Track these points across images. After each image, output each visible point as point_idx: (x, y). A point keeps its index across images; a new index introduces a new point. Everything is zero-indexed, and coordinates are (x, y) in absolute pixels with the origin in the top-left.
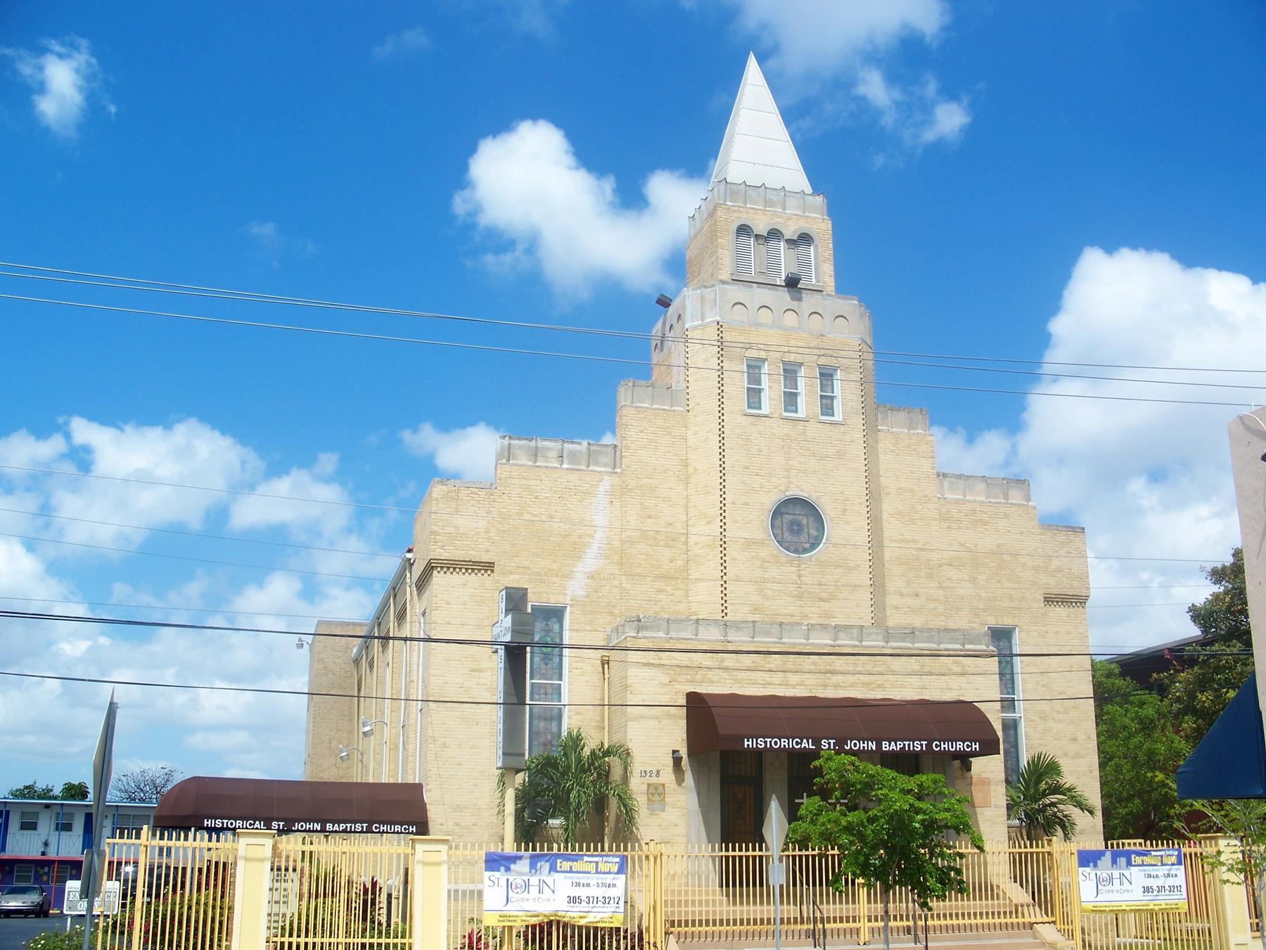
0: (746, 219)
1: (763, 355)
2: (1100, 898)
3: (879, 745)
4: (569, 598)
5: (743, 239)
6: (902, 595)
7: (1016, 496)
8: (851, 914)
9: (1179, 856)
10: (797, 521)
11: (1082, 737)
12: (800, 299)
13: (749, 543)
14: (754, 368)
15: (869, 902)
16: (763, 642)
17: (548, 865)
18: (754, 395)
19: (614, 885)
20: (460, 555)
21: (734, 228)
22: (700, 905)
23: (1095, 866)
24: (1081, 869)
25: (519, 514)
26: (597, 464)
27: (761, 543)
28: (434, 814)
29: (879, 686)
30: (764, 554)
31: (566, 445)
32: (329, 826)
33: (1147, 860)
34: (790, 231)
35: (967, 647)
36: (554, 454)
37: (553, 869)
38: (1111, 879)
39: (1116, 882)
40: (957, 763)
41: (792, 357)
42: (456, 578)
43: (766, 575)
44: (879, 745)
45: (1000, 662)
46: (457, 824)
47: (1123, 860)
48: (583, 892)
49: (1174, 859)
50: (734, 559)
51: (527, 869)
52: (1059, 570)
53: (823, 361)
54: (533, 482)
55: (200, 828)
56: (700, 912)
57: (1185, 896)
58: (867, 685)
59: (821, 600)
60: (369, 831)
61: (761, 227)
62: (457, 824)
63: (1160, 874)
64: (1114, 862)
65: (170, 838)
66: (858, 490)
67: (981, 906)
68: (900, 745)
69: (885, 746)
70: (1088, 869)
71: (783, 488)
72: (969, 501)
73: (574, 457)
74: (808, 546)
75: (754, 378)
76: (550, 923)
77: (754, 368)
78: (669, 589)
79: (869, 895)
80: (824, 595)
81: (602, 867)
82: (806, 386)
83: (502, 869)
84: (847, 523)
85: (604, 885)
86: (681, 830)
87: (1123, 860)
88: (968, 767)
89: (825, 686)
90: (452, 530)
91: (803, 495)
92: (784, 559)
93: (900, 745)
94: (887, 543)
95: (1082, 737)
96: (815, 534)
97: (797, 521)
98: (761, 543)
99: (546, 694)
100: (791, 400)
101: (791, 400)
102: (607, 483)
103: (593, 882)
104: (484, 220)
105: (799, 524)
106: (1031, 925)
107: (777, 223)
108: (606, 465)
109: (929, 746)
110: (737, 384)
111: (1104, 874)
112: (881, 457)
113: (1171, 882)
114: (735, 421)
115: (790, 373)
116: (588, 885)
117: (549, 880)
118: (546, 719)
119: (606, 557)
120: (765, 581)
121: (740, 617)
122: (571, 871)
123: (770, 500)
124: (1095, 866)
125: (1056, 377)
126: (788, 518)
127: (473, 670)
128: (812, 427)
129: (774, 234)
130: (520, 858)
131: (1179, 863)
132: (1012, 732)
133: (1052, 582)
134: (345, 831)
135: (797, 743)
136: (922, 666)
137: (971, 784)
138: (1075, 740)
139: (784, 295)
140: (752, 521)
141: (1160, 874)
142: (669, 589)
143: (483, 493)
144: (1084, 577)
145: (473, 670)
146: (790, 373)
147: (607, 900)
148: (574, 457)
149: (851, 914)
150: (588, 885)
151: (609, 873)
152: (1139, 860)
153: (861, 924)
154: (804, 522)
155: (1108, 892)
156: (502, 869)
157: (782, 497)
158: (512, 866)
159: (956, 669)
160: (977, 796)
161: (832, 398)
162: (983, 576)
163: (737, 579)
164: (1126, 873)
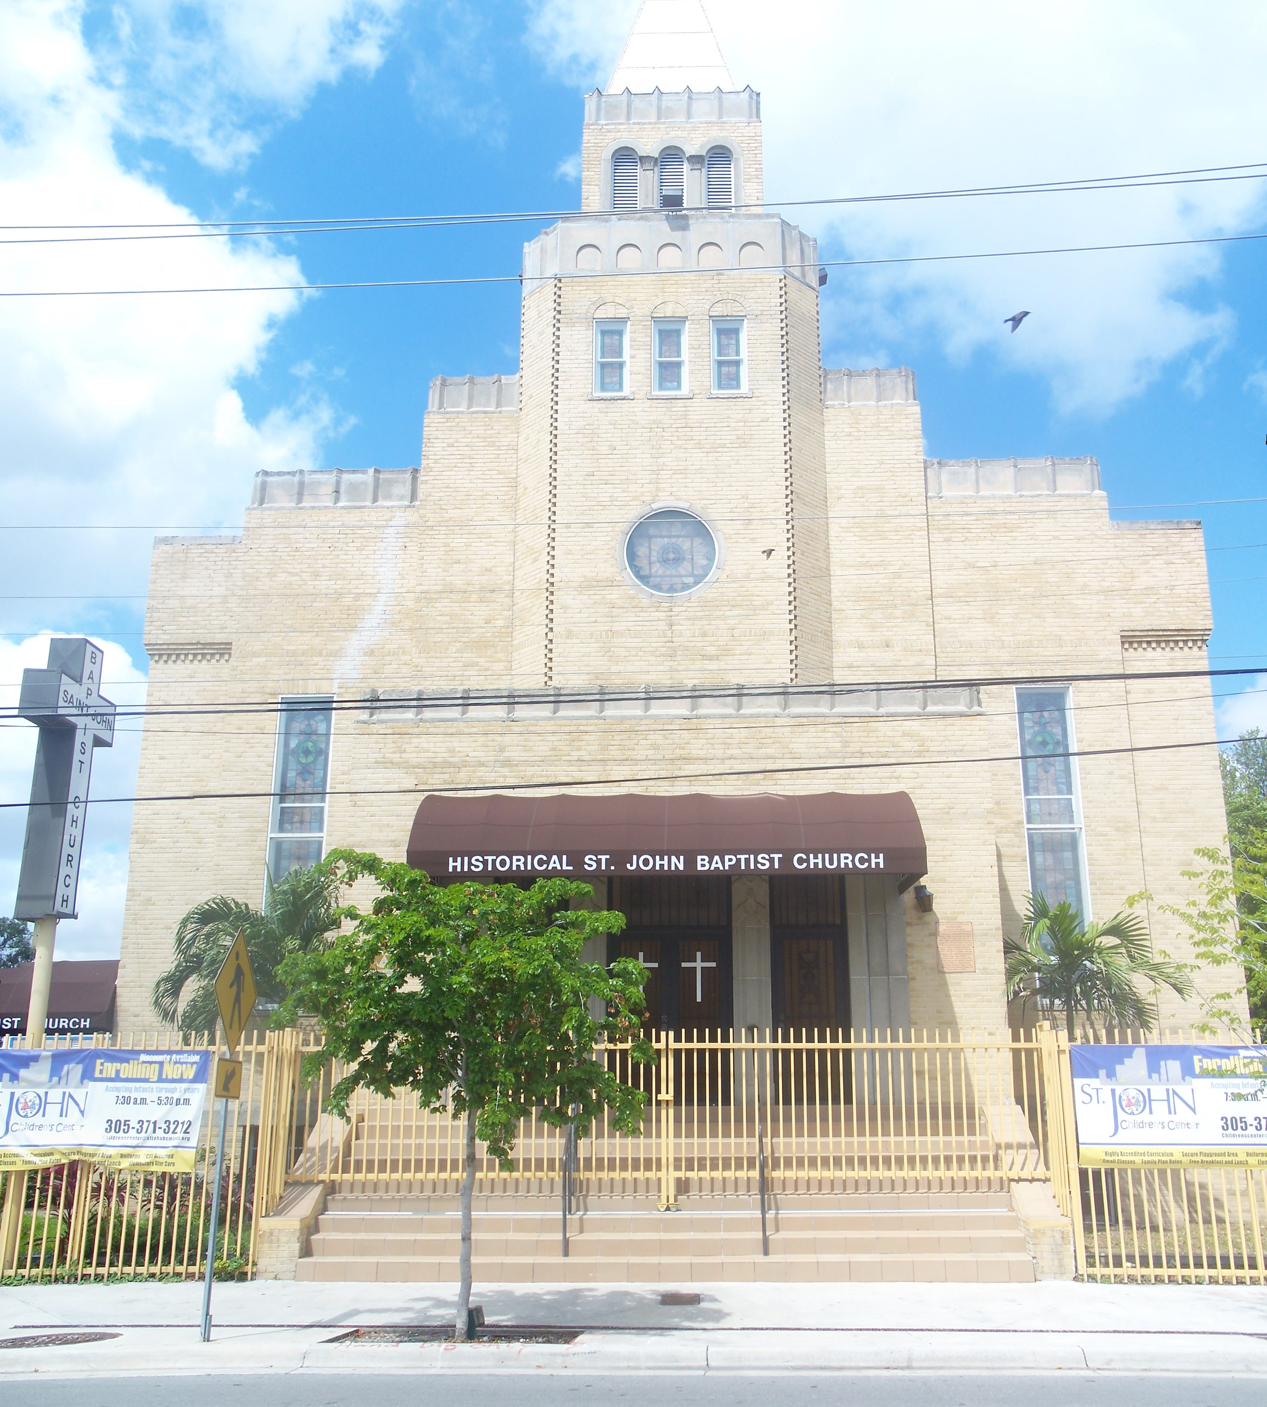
0: (625, 137)
1: (622, 313)
2: (1121, 1136)
3: (690, 862)
4: (336, 683)
5: (624, 169)
6: (861, 646)
8: (696, 1155)
12: (685, 228)
13: (589, 585)
14: (611, 332)
15: (677, 1134)
17: (80, 1068)
18: (610, 371)
19: (187, 1102)
20: (186, 636)
22: (396, 1135)
23: (1111, 1075)
24: (1078, 1082)
25: (272, 575)
26: (388, 497)
30: (614, 595)
31: (345, 476)
33: (126, 1070)
36: (330, 489)
37: (1188, 1071)
39: (1160, 1108)
41: (668, 311)
44: (690, 862)
45: (1067, 747)
48: (132, 1114)
50: (565, 608)
51: (45, 1077)
52: (1150, 590)
53: (718, 311)
56: (383, 1147)
66: (772, 492)
67: (960, 1145)
68: (730, 861)
69: (703, 864)
70: (1094, 1082)
71: (647, 498)
72: (983, 498)
73: (355, 490)
74: (691, 580)
76: (73, 1165)
77: (611, 332)
78: (481, 660)
79: (677, 1120)
80: (711, 650)
81: (170, 1071)
82: (696, 349)
83: (1102, 1073)
84: (753, 540)
87: (76, 1070)
91: (634, 513)
92: (645, 602)
93: (730, 861)
94: (835, 570)
96: (704, 562)
98: (611, 583)
99: (302, 822)
100: (669, 372)
101: (669, 372)
103: (151, 1096)
105: (676, 550)
106: (1004, 1185)
108: (402, 498)
109: (786, 861)
112: (830, 444)
115: (668, 333)
116: (144, 1101)
117: (79, 1094)
118: (299, 858)
122: (117, 1078)
124: (1111, 1075)
126: (658, 544)
131: (200, 1077)
132: (1068, 855)
135: (541, 862)
136: (846, 744)
137: (935, 934)
140: (595, 552)
142: (481, 660)
143: (222, 549)
146: (668, 333)
147: (170, 1126)
148: (355, 490)
149: (696, 1155)
150: (144, 1101)
151: (181, 1080)
152: (110, 1068)
153: (662, 1174)
154: (686, 545)
156: (1102, 1073)
157: (645, 510)
158: (23, 1073)
160: (948, 953)
161: (737, 363)
163: (569, 635)
164: (1183, 1090)
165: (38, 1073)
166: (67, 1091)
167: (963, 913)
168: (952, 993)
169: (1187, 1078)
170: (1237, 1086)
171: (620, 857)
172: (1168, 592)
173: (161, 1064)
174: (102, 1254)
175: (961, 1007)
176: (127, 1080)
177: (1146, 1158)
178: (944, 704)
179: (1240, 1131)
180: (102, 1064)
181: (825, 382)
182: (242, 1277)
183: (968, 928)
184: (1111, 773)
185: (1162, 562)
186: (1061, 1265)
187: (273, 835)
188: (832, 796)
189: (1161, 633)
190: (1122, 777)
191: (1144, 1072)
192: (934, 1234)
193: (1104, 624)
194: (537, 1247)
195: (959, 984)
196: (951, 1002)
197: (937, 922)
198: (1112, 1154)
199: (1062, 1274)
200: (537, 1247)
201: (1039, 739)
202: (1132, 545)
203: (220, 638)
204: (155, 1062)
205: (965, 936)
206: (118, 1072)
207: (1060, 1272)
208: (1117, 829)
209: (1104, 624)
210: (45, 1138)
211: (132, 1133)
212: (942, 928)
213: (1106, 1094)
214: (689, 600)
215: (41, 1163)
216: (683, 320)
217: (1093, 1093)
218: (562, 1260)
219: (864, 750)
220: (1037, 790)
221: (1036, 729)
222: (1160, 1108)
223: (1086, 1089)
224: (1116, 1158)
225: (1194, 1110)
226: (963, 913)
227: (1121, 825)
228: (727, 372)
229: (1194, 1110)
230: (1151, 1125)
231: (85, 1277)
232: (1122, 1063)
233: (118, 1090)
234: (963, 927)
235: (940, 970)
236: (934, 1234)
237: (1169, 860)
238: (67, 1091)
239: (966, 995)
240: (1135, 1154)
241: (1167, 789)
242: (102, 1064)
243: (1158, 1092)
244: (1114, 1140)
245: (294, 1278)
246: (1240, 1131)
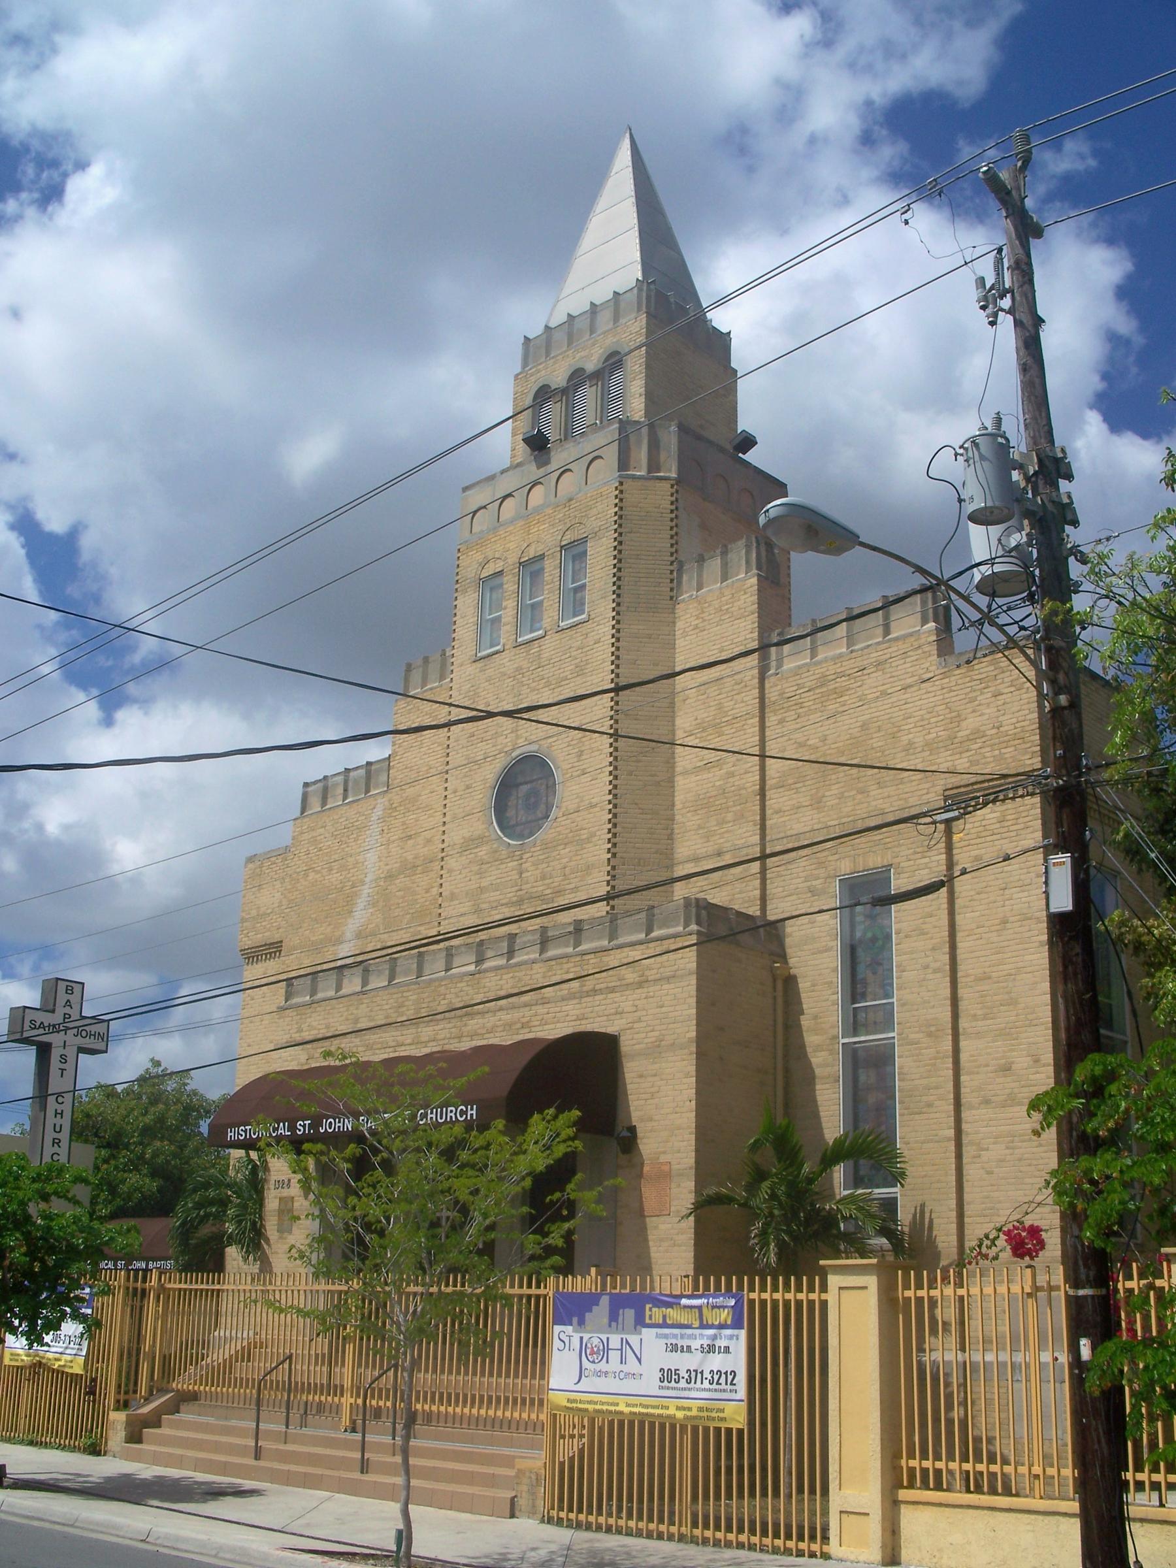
2: (584, 1385)
9: (737, 1310)
11: (1022, 1062)
23: (581, 1323)
27: (480, 840)
30: (483, 852)
33: (673, 1314)
38: (606, 1349)
39: (614, 1356)
43: (485, 883)
47: (629, 1314)
48: (683, 1363)
49: (725, 1316)
52: (977, 734)
57: (742, 1393)
58: (509, 1026)
63: (696, 1344)
64: (613, 1317)
65: (799, 1289)
70: (569, 1329)
83: (575, 1320)
87: (629, 1314)
89: (460, 1038)
95: (1022, 1062)
111: (594, 1339)
113: (716, 1362)
119: (374, 905)
120: (482, 890)
122: (664, 1325)
124: (581, 1323)
131: (737, 1325)
133: (962, 764)
137: (640, 1175)
138: (1007, 1069)
141: (696, 1344)
152: (656, 1314)
155: (599, 1374)
156: (575, 1320)
160: (649, 1193)
162: (835, 790)
164: (634, 1339)
165: (602, 1309)
166: (624, 1336)
167: (664, 1153)
168: (650, 1237)
169: (638, 1327)
170: (675, 1336)
172: (994, 731)
173: (700, 1308)
174: (590, 1506)
175: (657, 1252)
176: (673, 1326)
177: (598, 1407)
178: (668, 927)
179: (673, 1384)
180: (650, 1310)
181: (680, 577)
183: (666, 1168)
184: (927, 967)
185: (989, 695)
186: (534, 1506)
187: (846, 1040)
188: (264, 1079)
189: (986, 784)
190: (935, 971)
191: (606, 1320)
192: (490, 1470)
193: (927, 786)
194: (232, 1450)
195: (656, 1228)
196: (648, 1247)
197: (642, 1164)
198: (575, 1401)
199: (534, 1513)
200: (232, 1450)
201: (869, 935)
202: (960, 682)
204: (694, 1307)
205: (665, 1175)
206: (664, 1317)
207: (532, 1513)
208: (930, 1035)
209: (927, 786)
211: (683, 1384)
212: (646, 1169)
214: (534, 846)
216: (542, 557)
217: (567, 1340)
218: (253, 1462)
219: (598, 987)
220: (864, 997)
221: (867, 923)
223: (562, 1336)
224: (574, 1405)
225: (639, 1360)
226: (664, 1153)
227: (933, 1029)
228: (575, 599)
229: (639, 1360)
230: (606, 1373)
232: (591, 1311)
233: (666, 1336)
234: (663, 1167)
235: (641, 1214)
236: (490, 1470)
237: (987, 1065)
238: (624, 1336)
239: (661, 1240)
240: (590, 1402)
241: (990, 978)
242: (650, 1310)
244: (578, 1387)
246: (673, 1384)
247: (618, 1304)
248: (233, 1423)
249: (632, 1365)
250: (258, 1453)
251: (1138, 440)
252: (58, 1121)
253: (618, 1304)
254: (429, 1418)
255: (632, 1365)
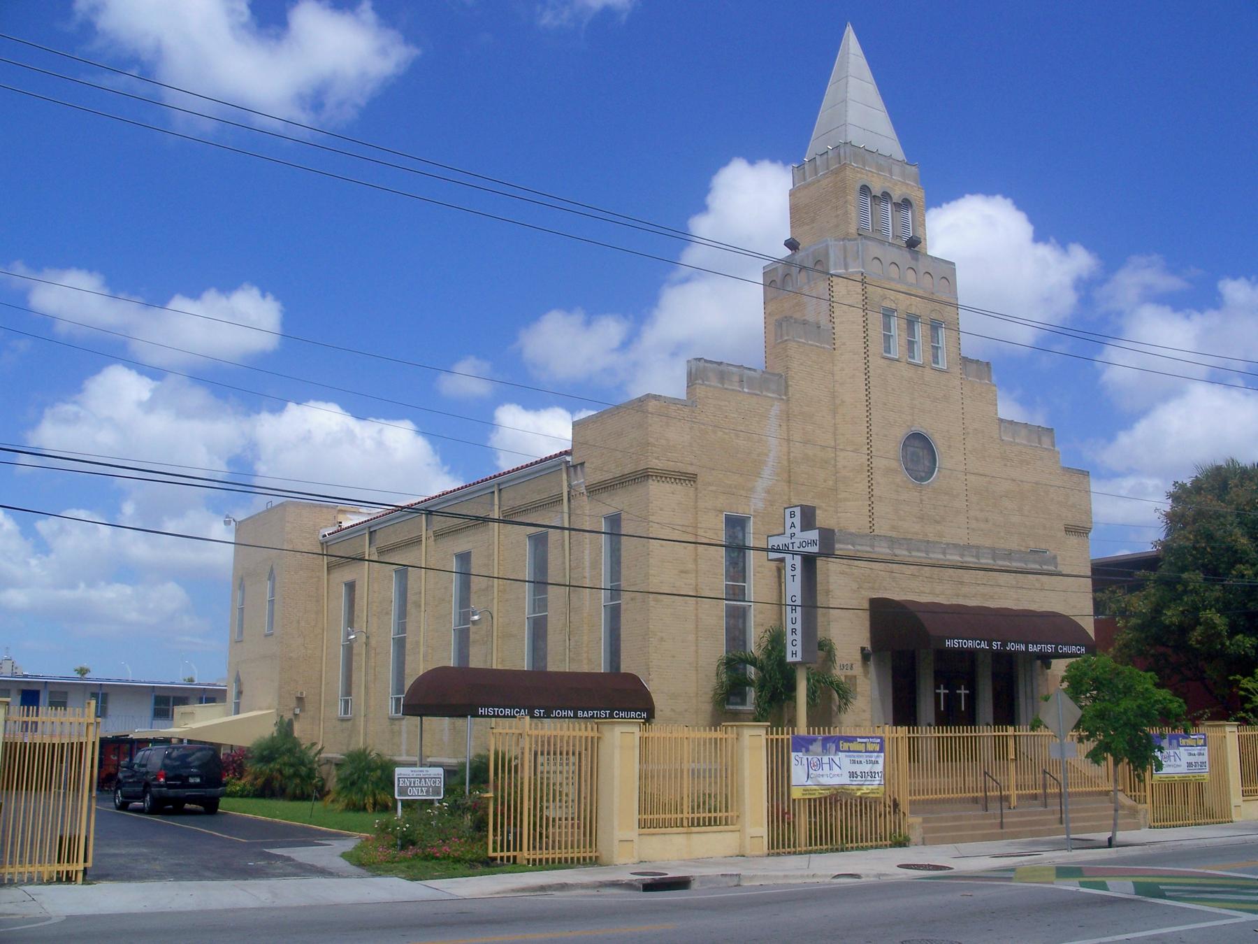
3: (1027, 648)
6: (977, 520)
7: (1046, 442)
10: (920, 452)
12: (917, 260)
16: (919, 555)
20: (671, 466)
21: (858, 187)
28: (659, 701)
29: (992, 597)
32: (580, 713)
33: (853, 746)
34: (897, 195)
35: (1045, 567)
36: (736, 378)
39: (826, 767)
40: (1039, 662)
42: (667, 487)
46: (673, 710)
48: (857, 768)
51: (820, 749)
54: (723, 403)
55: (475, 715)
59: (936, 521)
60: (611, 716)
61: (877, 189)
62: (673, 710)
63: (863, 760)
64: (824, 747)
69: (1011, 647)
70: (800, 754)
75: (887, 327)
80: (938, 518)
85: (871, 762)
86: (867, 715)
88: (1048, 666)
90: (663, 442)
91: (923, 431)
97: (920, 452)
102: (776, 409)
104: (105, 22)
107: (887, 186)
110: (876, 332)
114: (876, 362)
117: (836, 759)
121: (882, 533)
123: (900, 433)
125: (702, 272)
127: (682, 572)
128: (928, 371)
129: (886, 196)
130: (815, 740)
131: (881, 750)
134: (592, 717)
139: (906, 254)
144: (1088, 512)
145: (682, 572)
147: (873, 775)
152: (846, 746)
156: (1090, 745)
159: (1038, 585)
164: (836, 759)
165: (816, 747)
171: (1004, 645)
182: (905, 846)
203: (690, 469)
210: (825, 781)
213: (805, 761)
215: (827, 793)
222: (826, 767)
231: (847, 849)
243: (825, 759)
245: (924, 844)
247: (826, 740)
248: (113, 851)
249: (836, 770)
250: (1001, 825)
251: (126, 370)
252: (794, 649)
253: (826, 740)
254: (1070, 795)
255: (836, 770)
